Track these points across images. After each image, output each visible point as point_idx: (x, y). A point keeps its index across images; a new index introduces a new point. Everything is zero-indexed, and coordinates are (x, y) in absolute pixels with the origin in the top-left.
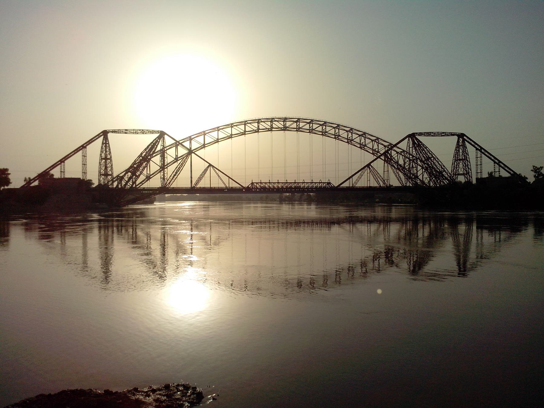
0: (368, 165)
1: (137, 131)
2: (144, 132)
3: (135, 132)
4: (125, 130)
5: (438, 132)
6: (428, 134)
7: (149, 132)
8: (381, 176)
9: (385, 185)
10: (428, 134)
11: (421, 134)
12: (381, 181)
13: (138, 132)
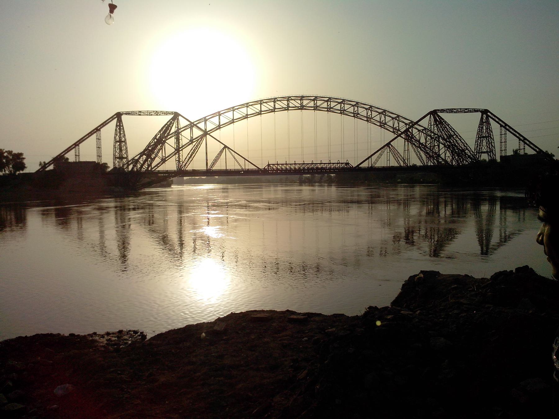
0: (388, 145)
1: (151, 112)
2: (158, 114)
3: (148, 113)
4: (139, 111)
5: (461, 109)
6: (451, 111)
7: (163, 114)
8: (401, 156)
9: (405, 165)
10: (451, 111)
11: (443, 111)
12: (402, 160)
13: (151, 113)
